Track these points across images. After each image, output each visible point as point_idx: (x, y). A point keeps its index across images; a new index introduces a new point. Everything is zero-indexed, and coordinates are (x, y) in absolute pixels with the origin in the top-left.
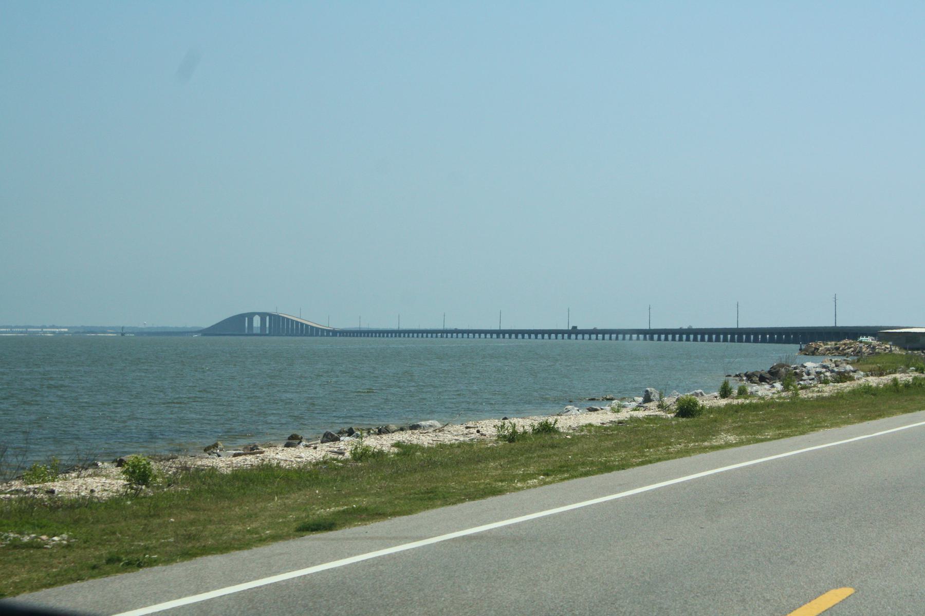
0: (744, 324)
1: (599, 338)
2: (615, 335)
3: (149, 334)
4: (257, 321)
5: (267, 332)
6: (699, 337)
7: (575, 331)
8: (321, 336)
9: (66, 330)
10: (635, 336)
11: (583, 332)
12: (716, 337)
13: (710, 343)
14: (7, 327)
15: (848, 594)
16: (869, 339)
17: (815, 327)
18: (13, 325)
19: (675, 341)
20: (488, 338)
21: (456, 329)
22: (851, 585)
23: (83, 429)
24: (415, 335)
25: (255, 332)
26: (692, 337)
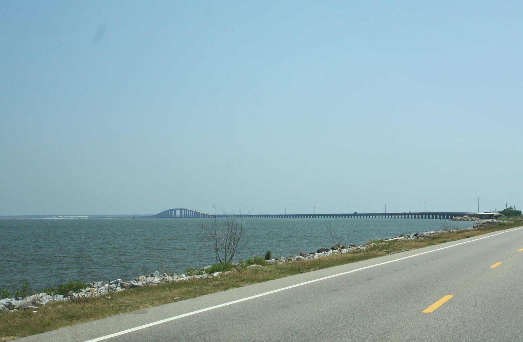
0: (428, 211)
1: (377, 217)
2: (404, 216)
3: (140, 217)
4: (178, 213)
5: (183, 216)
6: (434, 216)
7: (356, 214)
8: (208, 218)
9: (87, 216)
10: (393, 216)
11: (360, 215)
12: (435, 217)
13: (436, 219)
14: (68, 215)
15: (452, 297)
16: (466, 216)
17: (433, 213)
18: (77, 215)
19: (423, 218)
20: (371, 218)
21: (405, 213)
22: (452, 294)
23: (172, 268)
24: (249, 217)
25: (177, 216)
26: (427, 216)
